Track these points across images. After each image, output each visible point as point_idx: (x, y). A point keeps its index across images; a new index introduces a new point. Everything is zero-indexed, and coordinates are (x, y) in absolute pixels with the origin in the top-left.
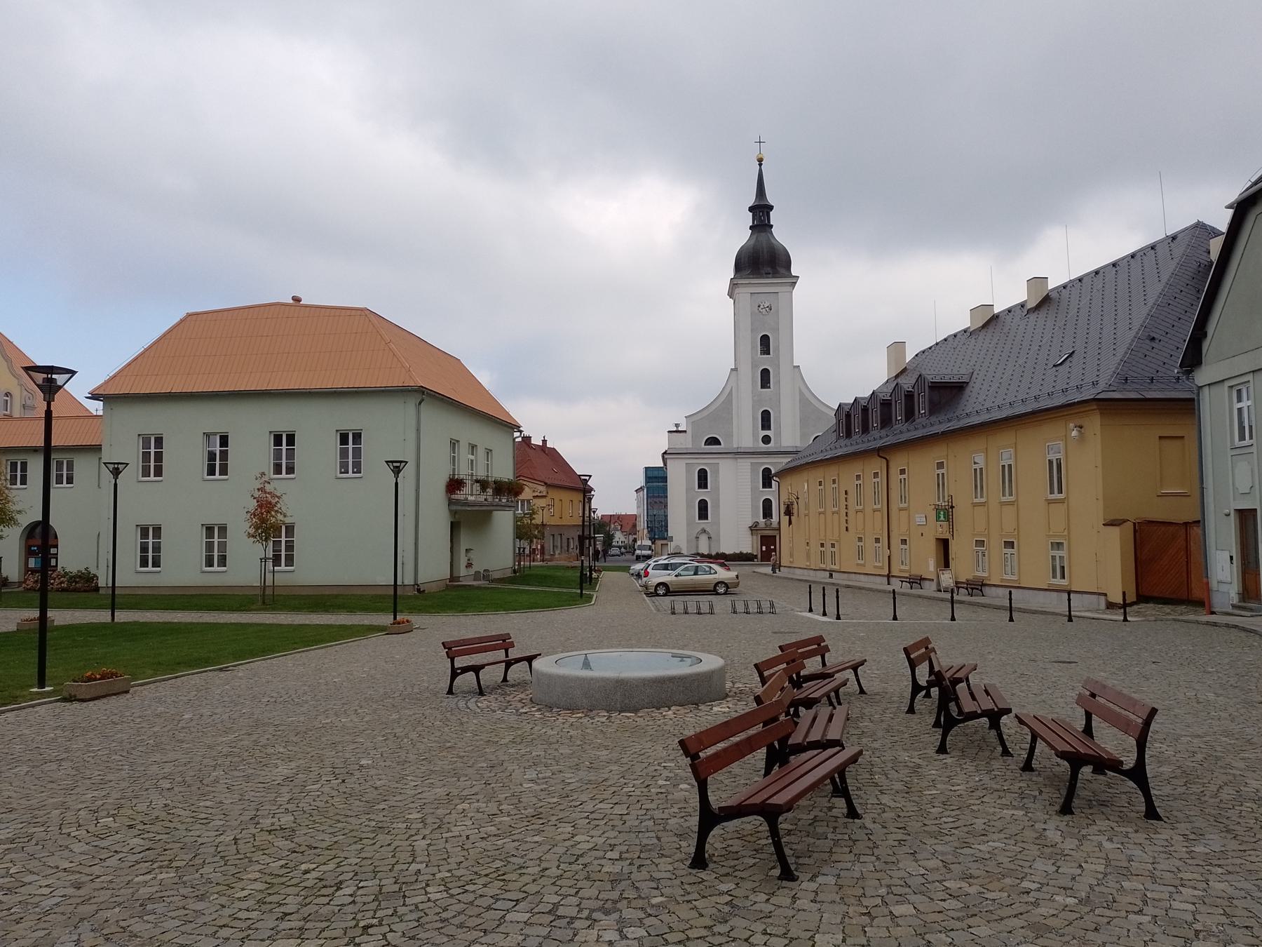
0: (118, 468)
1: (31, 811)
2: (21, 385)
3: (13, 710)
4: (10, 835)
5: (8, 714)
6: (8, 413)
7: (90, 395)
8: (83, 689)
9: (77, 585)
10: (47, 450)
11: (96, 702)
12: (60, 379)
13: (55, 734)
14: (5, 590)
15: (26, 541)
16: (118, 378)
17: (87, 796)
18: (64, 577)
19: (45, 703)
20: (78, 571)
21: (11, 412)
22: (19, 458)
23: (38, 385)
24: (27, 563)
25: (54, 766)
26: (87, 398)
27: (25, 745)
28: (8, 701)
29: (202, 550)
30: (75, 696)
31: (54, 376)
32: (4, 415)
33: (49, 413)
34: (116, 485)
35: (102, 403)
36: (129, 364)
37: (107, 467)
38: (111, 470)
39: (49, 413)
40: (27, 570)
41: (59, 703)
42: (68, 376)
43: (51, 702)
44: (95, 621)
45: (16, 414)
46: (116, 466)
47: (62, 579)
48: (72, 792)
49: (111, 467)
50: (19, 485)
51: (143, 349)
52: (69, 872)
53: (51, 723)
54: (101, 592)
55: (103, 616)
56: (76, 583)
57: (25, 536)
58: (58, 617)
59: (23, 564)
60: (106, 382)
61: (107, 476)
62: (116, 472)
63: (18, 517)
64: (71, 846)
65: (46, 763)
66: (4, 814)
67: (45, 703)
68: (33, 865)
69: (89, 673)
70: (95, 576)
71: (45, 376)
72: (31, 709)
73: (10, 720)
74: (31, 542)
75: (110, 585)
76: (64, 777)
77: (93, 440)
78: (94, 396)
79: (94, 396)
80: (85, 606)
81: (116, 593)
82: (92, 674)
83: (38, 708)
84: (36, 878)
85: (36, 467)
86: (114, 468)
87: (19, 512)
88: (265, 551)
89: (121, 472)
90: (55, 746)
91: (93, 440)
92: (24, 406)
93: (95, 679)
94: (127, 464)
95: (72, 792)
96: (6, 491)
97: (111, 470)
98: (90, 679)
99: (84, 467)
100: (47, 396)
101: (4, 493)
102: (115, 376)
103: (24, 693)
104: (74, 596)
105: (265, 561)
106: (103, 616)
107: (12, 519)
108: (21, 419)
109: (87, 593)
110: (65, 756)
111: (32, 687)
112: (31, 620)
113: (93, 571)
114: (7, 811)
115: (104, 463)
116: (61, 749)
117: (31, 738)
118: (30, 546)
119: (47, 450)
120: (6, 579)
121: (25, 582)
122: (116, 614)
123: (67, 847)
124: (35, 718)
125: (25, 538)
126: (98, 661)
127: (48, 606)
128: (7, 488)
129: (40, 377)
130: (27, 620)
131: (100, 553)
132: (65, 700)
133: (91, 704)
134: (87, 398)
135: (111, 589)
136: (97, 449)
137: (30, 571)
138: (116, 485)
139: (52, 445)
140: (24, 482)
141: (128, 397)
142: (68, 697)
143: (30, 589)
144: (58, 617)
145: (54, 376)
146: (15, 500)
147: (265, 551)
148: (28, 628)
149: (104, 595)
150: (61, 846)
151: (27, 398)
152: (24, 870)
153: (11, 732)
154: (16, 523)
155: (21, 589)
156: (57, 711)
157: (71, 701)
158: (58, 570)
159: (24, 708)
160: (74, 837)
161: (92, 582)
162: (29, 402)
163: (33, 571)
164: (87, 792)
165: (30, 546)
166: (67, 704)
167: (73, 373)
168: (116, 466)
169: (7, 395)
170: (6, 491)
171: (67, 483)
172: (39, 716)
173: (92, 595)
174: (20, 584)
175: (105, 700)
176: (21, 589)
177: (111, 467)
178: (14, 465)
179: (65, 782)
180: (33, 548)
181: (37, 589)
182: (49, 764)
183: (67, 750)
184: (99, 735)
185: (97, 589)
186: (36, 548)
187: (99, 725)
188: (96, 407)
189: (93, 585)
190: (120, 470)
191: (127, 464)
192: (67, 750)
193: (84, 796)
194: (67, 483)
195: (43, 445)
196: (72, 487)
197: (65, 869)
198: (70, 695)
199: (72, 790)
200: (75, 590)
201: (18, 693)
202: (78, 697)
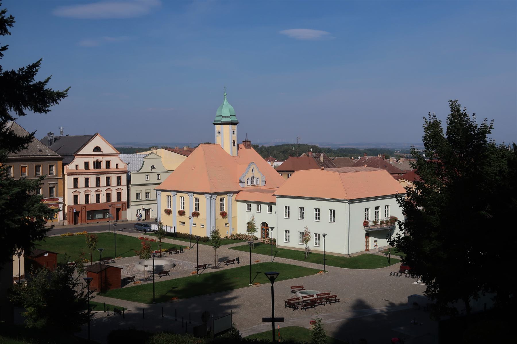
86: (271, 277)
129: (271, 228)
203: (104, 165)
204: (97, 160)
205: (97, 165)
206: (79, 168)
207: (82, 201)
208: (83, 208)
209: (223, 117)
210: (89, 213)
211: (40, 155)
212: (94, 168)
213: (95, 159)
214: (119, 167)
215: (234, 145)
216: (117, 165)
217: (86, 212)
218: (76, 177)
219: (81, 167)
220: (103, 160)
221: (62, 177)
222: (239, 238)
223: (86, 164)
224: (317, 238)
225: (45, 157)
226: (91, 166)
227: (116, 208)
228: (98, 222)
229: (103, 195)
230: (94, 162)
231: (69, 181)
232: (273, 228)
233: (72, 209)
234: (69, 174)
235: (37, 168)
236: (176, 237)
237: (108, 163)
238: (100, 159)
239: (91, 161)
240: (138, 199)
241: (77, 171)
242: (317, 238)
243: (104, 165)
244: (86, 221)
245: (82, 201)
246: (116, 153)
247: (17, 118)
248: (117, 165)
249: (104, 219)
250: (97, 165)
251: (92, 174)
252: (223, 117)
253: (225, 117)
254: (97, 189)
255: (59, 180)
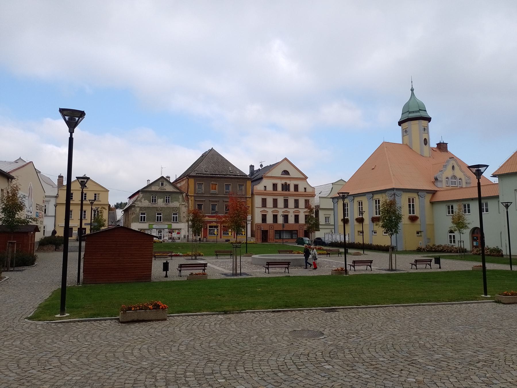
0: (508, 205)
1: (491, 350)
2: (465, 175)
3: (476, 303)
4: (484, 358)
5: (474, 304)
6: (461, 186)
7: (492, 176)
8: (504, 298)
9: (494, 253)
10: (480, 199)
11: (510, 305)
12: (482, 169)
13: (495, 317)
14: (466, 254)
15: (472, 235)
16: (503, 167)
17: (515, 349)
18: (488, 250)
19: (488, 302)
20: (494, 248)
21: (462, 185)
22: (466, 203)
23: (474, 173)
24: (473, 243)
25: (497, 331)
26: (491, 177)
27: (483, 319)
28: (474, 299)
29: (448, 238)
30: (500, 301)
31: (480, 169)
32: (460, 187)
33: (479, 184)
34: (507, 212)
35: (498, 178)
36: (508, 161)
37: (502, 204)
38: (505, 205)
39: (479, 184)
40: (473, 246)
41: (494, 303)
42: (485, 168)
43: (490, 302)
44: (503, 269)
45: (464, 186)
46: (507, 204)
47: (487, 250)
48: (507, 345)
49: (505, 204)
50: (467, 213)
51: (514, 153)
52: (512, 384)
53: (492, 311)
54: (505, 257)
55: (507, 267)
56: (493, 252)
57: (471, 232)
58: (489, 266)
59: (471, 245)
60: (499, 169)
61: (503, 208)
62: (507, 206)
63: (468, 226)
64: (512, 372)
65: (493, 329)
66: (480, 348)
67: (488, 302)
68: (495, 375)
69: (506, 292)
70: (501, 250)
71: (476, 169)
72: (482, 304)
73: (475, 307)
74: (474, 235)
75: (508, 254)
76: (502, 337)
77: (484, 195)
78: (494, 176)
79: (494, 176)
80: (498, 262)
81: (512, 258)
82: (507, 293)
83: (486, 304)
84: (499, 382)
85: (474, 207)
86: (506, 205)
87: (469, 224)
88: (391, 238)
89: (509, 206)
90: (496, 322)
91: (484, 195)
92: (466, 183)
93: (509, 295)
94: (512, 202)
95: (507, 345)
96: (463, 216)
97: (505, 205)
98: (506, 295)
99: (492, 205)
100: (478, 177)
101: (463, 216)
102: (502, 166)
103: (480, 296)
104: (493, 258)
105: (461, 242)
106: (507, 267)
107: (466, 226)
108: (466, 188)
109: (498, 257)
110: (501, 327)
111: (482, 294)
112: (477, 266)
113: (500, 248)
114: (481, 347)
115: (502, 203)
116: (498, 324)
117: (485, 316)
118: (474, 237)
119: (480, 199)
120: (466, 249)
121: (473, 251)
122: (512, 267)
123: (509, 371)
124: (485, 308)
125: (471, 234)
126: (508, 287)
127: (486, 262)
128: (464, 215)
129: (474, 170)
130: (476, 266)
131: (502, 241)
132: (496, 302)
133: (508, 306)
134: (491, 177)
135: (509, 256)
136: (497, 197)
137: (475, 247)
138: (507, 212)
139: (482, 196)
140: (469, 212)
141: (508, 174)
142: (498, 301)
143: (475, 254)
144: (489, 266)
145: (480, 169)
146: (467, 219)
147: (391, 238)
148: (476, 269)
149: (506, 258)
150: (506, 370)
151: (467, 180)
152: (492, 377)
153: (476, 312)
154: (468, 228)
155: (472, 254)
156: (494, 306)
157: (499, 303)
158: (486, 247)
159: (480, 303)
160: (512, 367)
161: (500, 252)
162: (468, 181)
163: (476, 247)
164: (514, 347)
165: (474, 237)
166: (497, 304)
167: (487, 166)
168: (507, 204)
169: (460, 179)
170: (463, 216)
171: (486, 212)
172: (487, 307)
173: (500, 258)
174: (471, 252)
175: (514, 305)
176: (472, 254)
177: (505, 204)
178: (465, 206)
179: (503, 340)
180: (474, 238)
181: (478, 254)
182: (494, 330)
183: (501, 325)
184: (515, 321)
185: (502, 256)
186: (476, 238)
187: (514, 316)
188: (495, 180)
189: (501, 254)
190: (509, 205)
191: (512, 202)
192: (501, 325)
193: (513, 349)
194: (486, 212)
195: (478, 197)
196: (470, 215)
197: (510, 382)
198: (498, 300)
199: (507, 344)
200: (493, 255)
201: (477, 296)
202: (502, 302)
203: (292, 188)
204: (286, 183)
205: (285, 187)
206: (267, 189)
207: (270, 220)
208: (271, 227)
209: (410, 112)
210: (276, 232)
211: (230, 175)
212: (283, 190)
213: (283, 182)
214: (307, 190)
215: (426, 145)
216: (305, 189)
217: (274, 231)
218: (264, 197)
219: (270, 188)
220: (292, 184)
221: (250, 196)
222: (265, 288)
223: (275, 186)
224: (154, 198)
225: (234, 176)
226: (279, 188)
227: (304, 230)
228: (286, 242)
229: (291, 216)
230: (282, 185)
231: (258, 200)
232: (482, 169)
233: (260, 228)
234: (260, 194)
235: (228, 186)
236: (39, 245)
237: (296, 187)
238: (288, 182)
239: (279, 183)
240: (327, 223)
241: (265, 192)
242: (154, 198)
243: (292, 188)
244: (274, 239)
245: (270, 220)
246: (304, 177)
247: (321, 191)
248: (305, 189)
249: (292, 239)
250: (285, 187)
251: (280, 195)
252: (410, 112)
253: (413, 112)
254: (285, 209)
255: (248, 199)
